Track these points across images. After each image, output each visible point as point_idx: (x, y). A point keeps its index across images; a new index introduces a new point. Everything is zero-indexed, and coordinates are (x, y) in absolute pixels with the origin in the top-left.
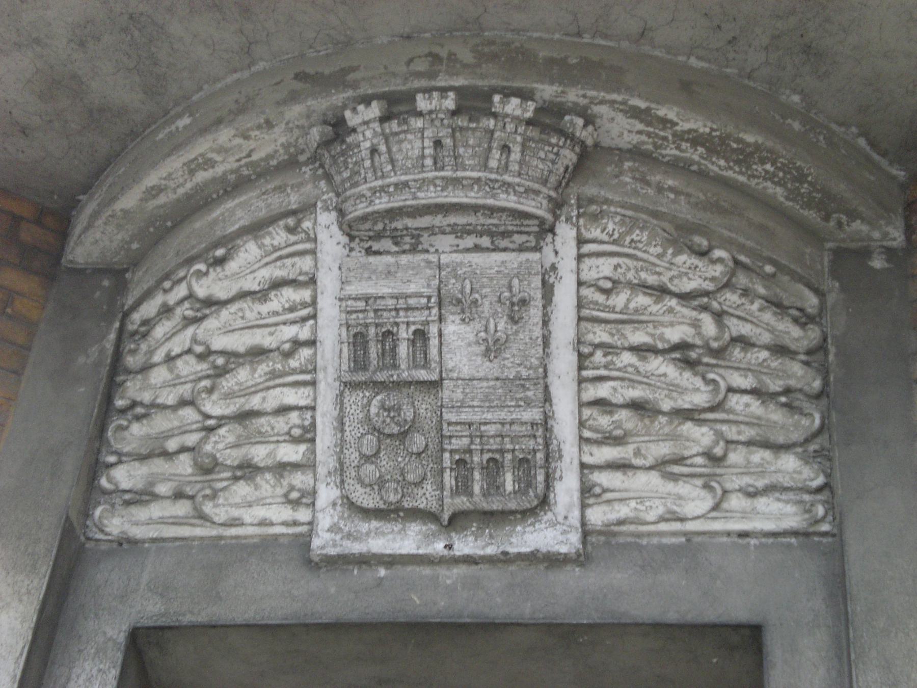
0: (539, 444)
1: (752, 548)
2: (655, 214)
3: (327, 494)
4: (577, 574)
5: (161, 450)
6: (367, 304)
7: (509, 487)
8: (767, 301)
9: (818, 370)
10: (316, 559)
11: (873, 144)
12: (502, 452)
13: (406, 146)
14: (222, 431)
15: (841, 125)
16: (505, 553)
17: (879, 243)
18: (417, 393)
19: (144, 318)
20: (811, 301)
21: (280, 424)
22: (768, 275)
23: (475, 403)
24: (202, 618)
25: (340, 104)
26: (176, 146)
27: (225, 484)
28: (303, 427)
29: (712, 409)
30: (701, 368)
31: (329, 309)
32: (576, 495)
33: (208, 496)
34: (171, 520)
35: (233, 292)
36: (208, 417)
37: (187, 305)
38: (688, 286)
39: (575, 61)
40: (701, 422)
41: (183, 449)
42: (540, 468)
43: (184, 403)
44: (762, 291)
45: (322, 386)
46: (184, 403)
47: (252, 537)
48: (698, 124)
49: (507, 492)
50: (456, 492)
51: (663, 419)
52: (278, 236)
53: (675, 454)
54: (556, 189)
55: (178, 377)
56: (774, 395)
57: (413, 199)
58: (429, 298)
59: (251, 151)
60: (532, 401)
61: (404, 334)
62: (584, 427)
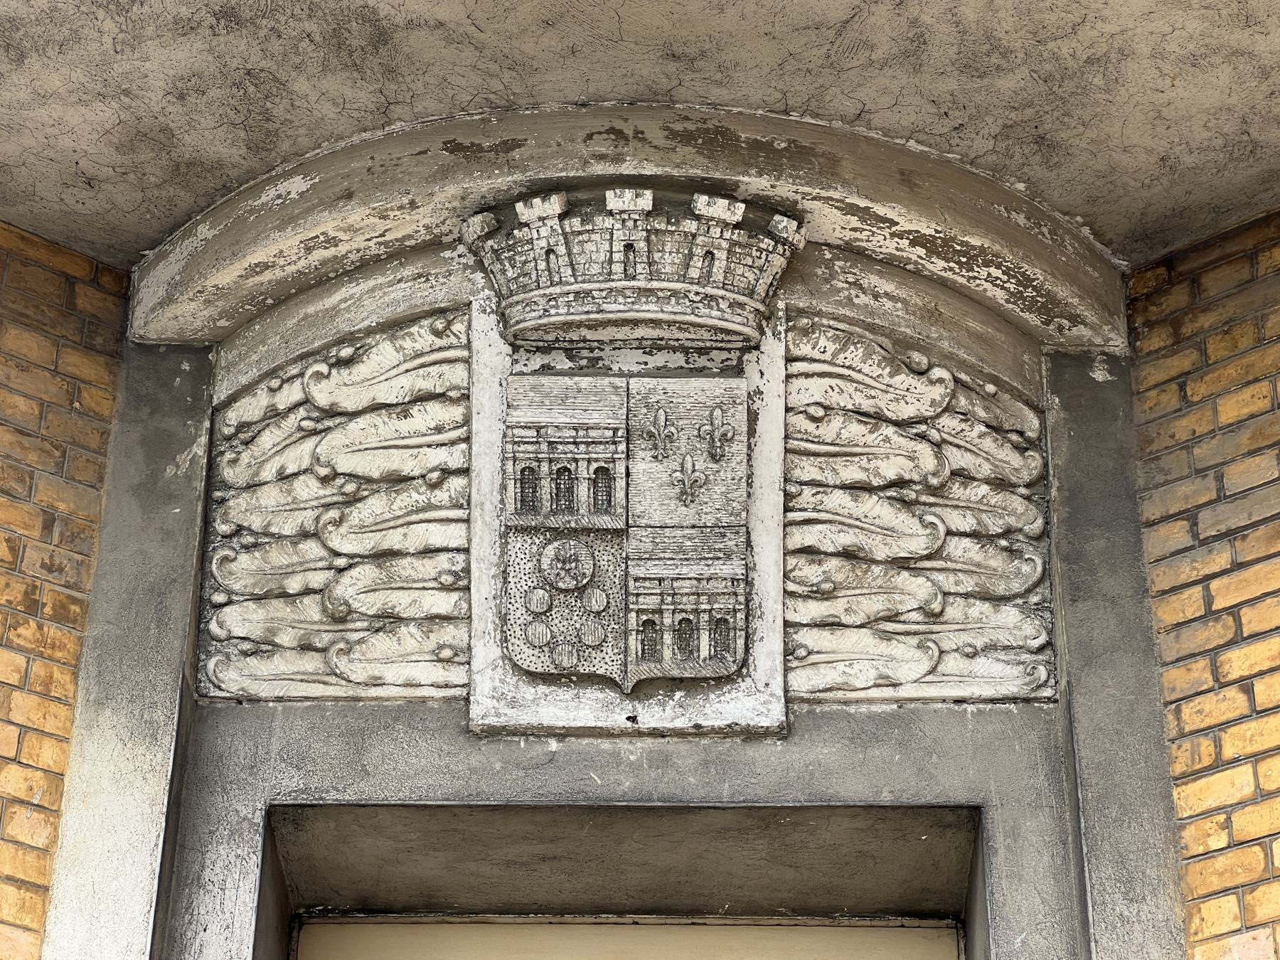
0: (740, 603)
1: (969, 716)
2: (872, 328)
3: (486, 652)
4: (779, 748)
5: (281, 590)
6: (539, 435)
7: (704, 653)
8: (988, 426)
9: (1038, 505)
10: (478, 730)
11: (1096, 234)
12: (696, 612)
13: (589, 247)
14: (354, 572)
15: (1065, 214)
16: (697, 726)
17: (1101, 349)
18: (599, 542)
19: (243, 420)
20: (1032, 424)
21: (428, 568)
22: (988, 394)
23: (667, 555)
24: (349, 796)
25: (505, 188)
26: (288, 216)
27: (362, 634)
28: (455, 574)
29: (928, 557)
30: (918, 510)
31: (487, 433)
32: (780, 658)
33: (342, 650)
34: (299, 677)
35: (364, 403)
36: (338, 554)
37: (302, 412)
38: (907, 412)
39: (783, 145)
40: (917, 572)
41: (308, 592)
42: (740, 630)
43: (304, 535)
44: (982, 413)
45: (477, 526)
46: (304, 535)
47: (395, 699)
48: (926, 228)
49: (702, 657)
50: (643, 657)
51: (877, 570)
52: (421, 337)
53: (889, 609)
54: (763, 302)
55: (295, 500)
56: (992, 538)
57: (598, 313)
58: (615, 430)
59: (386, 231)
60: (733, 552)
61: (584, 471)
62: (789, 579)
